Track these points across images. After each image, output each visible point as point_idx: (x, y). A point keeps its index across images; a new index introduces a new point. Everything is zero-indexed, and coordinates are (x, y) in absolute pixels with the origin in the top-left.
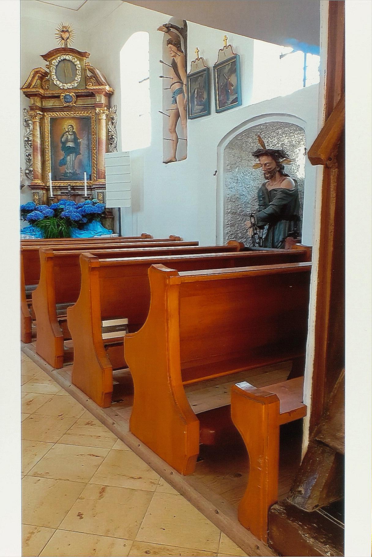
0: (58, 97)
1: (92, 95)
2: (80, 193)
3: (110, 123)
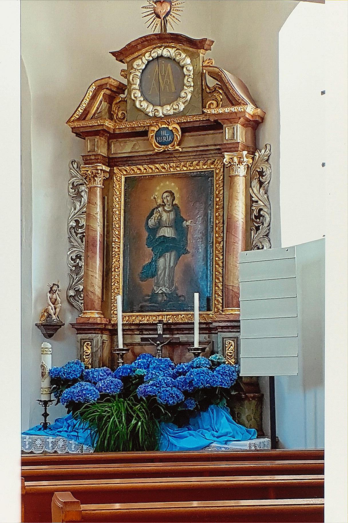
0: (144, 134)
1: (216, 125)
2: (183, 338)
3: (255, 183)
